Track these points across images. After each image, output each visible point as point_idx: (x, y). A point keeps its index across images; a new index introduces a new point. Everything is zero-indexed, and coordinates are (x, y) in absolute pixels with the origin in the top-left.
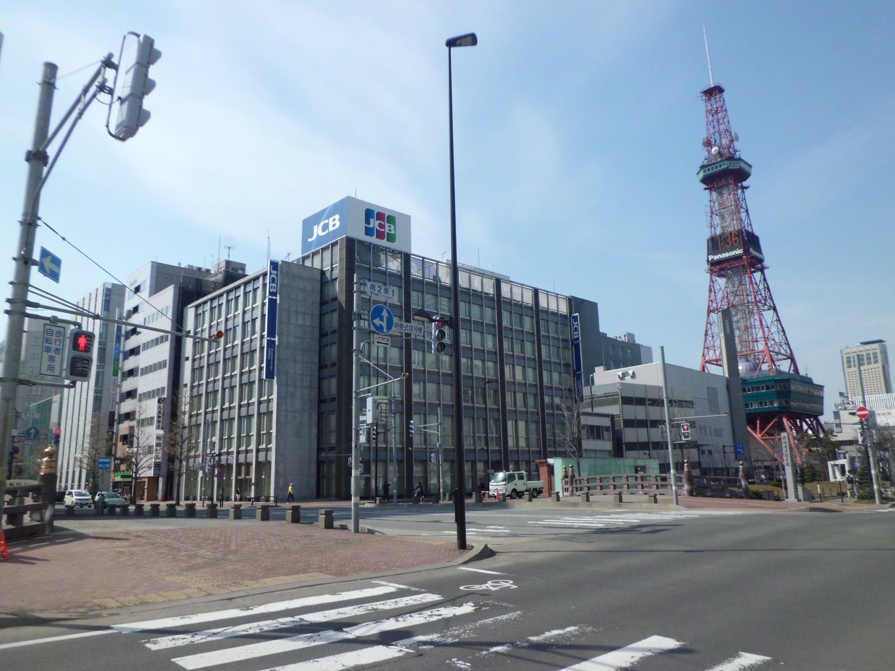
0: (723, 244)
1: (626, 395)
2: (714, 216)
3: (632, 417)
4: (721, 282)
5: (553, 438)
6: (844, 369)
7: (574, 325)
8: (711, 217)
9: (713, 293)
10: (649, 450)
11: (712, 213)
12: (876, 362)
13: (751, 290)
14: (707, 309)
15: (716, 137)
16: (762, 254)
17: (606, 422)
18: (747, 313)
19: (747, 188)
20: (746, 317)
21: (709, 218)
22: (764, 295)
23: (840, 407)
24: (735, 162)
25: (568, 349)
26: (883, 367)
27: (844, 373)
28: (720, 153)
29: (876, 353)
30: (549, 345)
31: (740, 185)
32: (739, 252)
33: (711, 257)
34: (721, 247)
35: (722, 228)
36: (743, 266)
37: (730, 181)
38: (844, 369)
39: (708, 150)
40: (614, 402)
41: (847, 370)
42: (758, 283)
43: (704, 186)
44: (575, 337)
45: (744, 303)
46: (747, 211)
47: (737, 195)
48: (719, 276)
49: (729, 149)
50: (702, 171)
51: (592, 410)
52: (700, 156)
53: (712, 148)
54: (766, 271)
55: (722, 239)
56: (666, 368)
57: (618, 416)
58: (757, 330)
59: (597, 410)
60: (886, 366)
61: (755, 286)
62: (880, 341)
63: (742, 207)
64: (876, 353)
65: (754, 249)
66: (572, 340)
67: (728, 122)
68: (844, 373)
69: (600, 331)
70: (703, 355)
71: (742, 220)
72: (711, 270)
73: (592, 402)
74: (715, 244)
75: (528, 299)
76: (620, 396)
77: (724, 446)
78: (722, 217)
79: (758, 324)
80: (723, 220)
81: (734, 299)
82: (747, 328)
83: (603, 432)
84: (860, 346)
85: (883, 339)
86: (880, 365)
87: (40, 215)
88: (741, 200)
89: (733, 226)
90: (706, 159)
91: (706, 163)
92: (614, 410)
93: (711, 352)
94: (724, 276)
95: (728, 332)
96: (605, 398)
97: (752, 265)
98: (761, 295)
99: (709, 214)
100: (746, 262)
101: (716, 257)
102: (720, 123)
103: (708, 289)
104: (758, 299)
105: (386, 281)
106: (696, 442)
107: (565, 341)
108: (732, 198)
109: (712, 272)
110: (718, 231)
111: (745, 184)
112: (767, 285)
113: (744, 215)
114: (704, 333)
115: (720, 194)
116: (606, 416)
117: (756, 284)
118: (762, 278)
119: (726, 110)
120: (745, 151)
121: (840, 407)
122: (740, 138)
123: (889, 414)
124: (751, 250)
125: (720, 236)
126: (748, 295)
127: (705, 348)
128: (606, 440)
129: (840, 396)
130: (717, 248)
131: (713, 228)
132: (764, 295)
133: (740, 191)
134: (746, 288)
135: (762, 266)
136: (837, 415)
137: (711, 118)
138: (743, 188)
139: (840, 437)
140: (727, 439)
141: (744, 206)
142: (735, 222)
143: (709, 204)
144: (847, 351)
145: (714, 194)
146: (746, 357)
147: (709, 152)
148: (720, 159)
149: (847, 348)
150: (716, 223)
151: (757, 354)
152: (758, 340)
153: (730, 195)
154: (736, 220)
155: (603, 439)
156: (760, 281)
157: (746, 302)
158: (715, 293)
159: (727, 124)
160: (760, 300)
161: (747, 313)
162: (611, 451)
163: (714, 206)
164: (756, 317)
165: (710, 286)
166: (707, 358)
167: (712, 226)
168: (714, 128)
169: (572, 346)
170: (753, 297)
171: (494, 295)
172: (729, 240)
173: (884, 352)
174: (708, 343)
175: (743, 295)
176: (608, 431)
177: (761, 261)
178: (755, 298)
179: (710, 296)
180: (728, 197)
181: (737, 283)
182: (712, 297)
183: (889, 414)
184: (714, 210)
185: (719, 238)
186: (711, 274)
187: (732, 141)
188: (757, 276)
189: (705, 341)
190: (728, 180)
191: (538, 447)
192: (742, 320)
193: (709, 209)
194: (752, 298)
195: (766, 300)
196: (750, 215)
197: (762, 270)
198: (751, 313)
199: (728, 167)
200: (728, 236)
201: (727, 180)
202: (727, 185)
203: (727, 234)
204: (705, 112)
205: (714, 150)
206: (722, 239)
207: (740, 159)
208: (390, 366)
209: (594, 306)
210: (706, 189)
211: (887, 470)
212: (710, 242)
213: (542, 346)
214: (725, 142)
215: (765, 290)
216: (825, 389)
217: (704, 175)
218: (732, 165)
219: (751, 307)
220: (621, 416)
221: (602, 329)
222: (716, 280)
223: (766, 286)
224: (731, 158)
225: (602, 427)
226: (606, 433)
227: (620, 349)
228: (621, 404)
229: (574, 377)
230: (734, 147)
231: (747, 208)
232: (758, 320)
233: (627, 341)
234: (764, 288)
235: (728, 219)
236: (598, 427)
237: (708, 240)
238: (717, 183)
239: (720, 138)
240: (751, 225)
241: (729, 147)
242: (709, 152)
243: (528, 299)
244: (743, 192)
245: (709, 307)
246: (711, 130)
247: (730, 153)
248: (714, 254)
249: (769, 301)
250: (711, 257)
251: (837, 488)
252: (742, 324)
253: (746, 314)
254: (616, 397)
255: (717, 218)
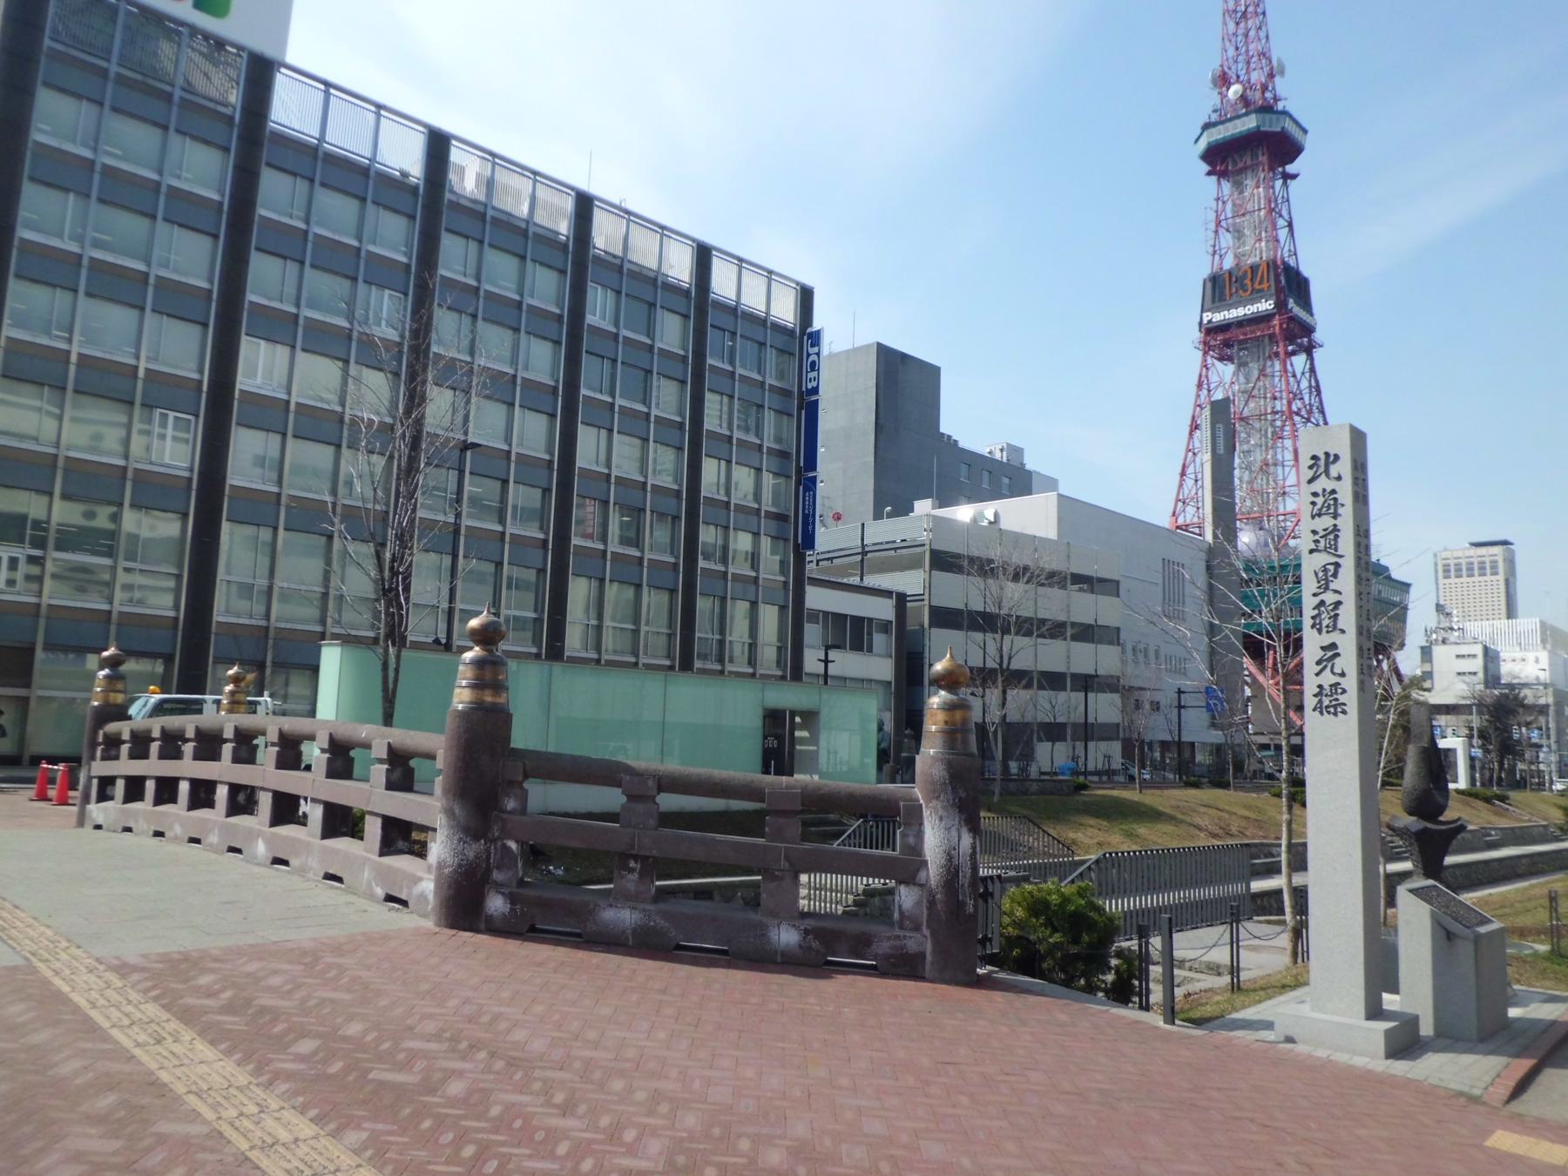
0: (1234, 290)
1: (941, 546)
2: (1221, 231)
3: (956, 603)
4: (1226, 370)
5: (717, 637)
6: (1437, 579)
7: (809, 355)
8: (1216, 232)
9: (1205, 392)
10: (375, 510)
11: (1218, 223)
12: (1496, 573)
13: (1284, 387)
14: (1189, 422)
15: (1240, 68)
16: (1312, 315)
17: (884, 610)
18: (1269, 435)
19: (1294, 177)
20: (1267, 443)
21: (1212, 235)
22: (1307, 402)
23: (1434, 636)
24: (1274, 117)
25: (790, 415)
26: (1507, 581)
27: (1437, 584)
28: (1243, 98)
29: (1496, 562)
30: (731, 397)
31: (1280, 169)
32: (1266, 306)
33: (1207, 316)
34: (1231, 295)
35: (1236, 256)
36: (1272, 337)
37: (1260, 159)
38: (1437, 579)
39: (1220, 93)
40: (913, 564)
41: (1442, 581)
42: (1299, 375)
43: (1205, 168)
44: (809, 387)
45: (1266, 414)
46: (1290, 225)
47: (1273, 187)
48: (1221, 359)
49: (1263, 93)
50: (1205, 134)
51: (862, 579)
52: (1206, 102)
53: (1228, 89)
54: (1317, 354)
55: (1234, 279)
56: (1068, 506)
57: (918, 598)
58: (1287, 469)
59: (872, 580)
60: (1511, 579)
61: (1292, 379)
62: (1505, 543)
63: (1281, 216)
64: (1496, 562)
65: (1295, 302)
66: (800, 392)
67: (1267, 37)
68: (1437, 584)
69: (942, 430)
70: (1174, 514)
71: (1278, 241)
72: (1205, 343)
73: (862, 561)
74: (1219, 288)
75: (680, 268)
76: (927, 547)
77: (1180, 692)
78: (1238, 234)
79: (1289, 456)
80: (1239, 239)
81: (1246, 404)
82: (1267, 465)
83: (870, 634)
84: (1468, 549)
85: (1510, 540)
86: (1501, 577)
87: (340, 372)
88: (1280, 201)
89: (1257, 252)
90: (1215, 111)
91: (1214, 117)
92: (911, 582)
93: (1190, 510)
94: (1230, 359)
95: (1221, 450)
96: (893, 552)
97: (1290, 337)
98: (1302, 399)
99: (1212, 226)
100: (1277, 328)
101: (1218, 317)
102: (1253, 66)
103: (1195, 381)
104: (1294, 408)
105: (761, 463)
106: (1118, 678)
107: (786, 393)
108: (1262, 195)
109: (1207, 347)
110: (1229, 263)
111: (1290, 168)
112: (1317, 381)
113: (1283, 234)
114: (1179, 470)
115: (1239, 186)
116: (887, 593)
117: (1294, 376)
118: (1308, 366)
119: (1264, 13)
120: (1294, 96)
121: (1434, 636)
122: (1288, 71)
123: (1524, 660)
124: (1291, 303)
125: (1230, 273)
126: (1275, 398)
127: (1178, 500)
128: (879, 655)
129: (1437, 611)
130: (1222, 299)
131: (1217, 257)
132: (1307, 402)
133: (1279, 183)
134: (1274, 387)
135: (1310, 341)
136: (1426, 653)
137: (1231, 26)
138: (1287, 177)
139: (1434, 699)
140: (1199, 673)
141: (1285, 213)
142: (1263, 244)
143: (1214, 204)
144: (1444, 555)
145: (1227, 187)
146: (1258, 523)
147: (1223, 96)
148: (1244, 111)
149: (1445, 550)
150: (1224, 244)
151: (1281, 518)
152: (1287, 490)
153: (1258, 187)
154: (1268, 241)
155: (870, 650)
156: (1303, 373)
157: (1269, 411)
158: (1209, 391)
159: (1264, 41)
160: (1299, 409)
161: (1269, 435)
162: (890, 683)
163: (1224, 210)
164: (1288, 443)
165: (1200, 375)
166: (1181, 521)
167: (1215, 252)
168: (1237, 49)
169: (800, 408)
170: (1285, 402)
171: (568, 238)
172: (1247, 281)
173: (1510, 562)
174: (1186, 492)
175: (1265, 398)
176: (886, 632)
177: (1308, 330)
178: (1290, 403)
179: (1198, 396)
180: (1255, 191)
181: (1256, 373)
182: (1202, 398)
183: (1524, 660)
184: (1223, 217)
185: (1227, 276)
186: (1205, 353)
187: (1271, 76)
188: (1299, 361)
189: (1181, 486)
190: (1257, 157)
191: (668, 657)
192: (1258, 449)
193: (1212, 216)
194: (1282, 405)
195: (1310, 412)
196: (1296, 235)
197: (1309, 350)
198: (1278, 436)
199: (1258, 127)
200: (1246, 272)
201: (1254, 156)
202: (1253, 168)
203: (1244, 268)
204: (1221, 13)
205: (1234, 90)
206: (1234, 279)
207: (1285, 113)
208: (732, 574)
209: (930, 374)
210: (1209, 174)
211: (832, 816)
212: (1209, 285)
213: (708, 396)
214: (1257, 77)
215: (1311, 393)
216: (1412, 590)
217: (1209, 143)
218: (1267, 124)
219: (1278, 423)
220: (926, 597)
221: (949, 424)
222: (1213, 364)
223: (1313, 384)
224: (1267, 109)
225: (870, 620)
226: (879, 640)
227: (986, 474)
228: (927, 568)
229: (798, 483)
230: (1274, 88)
231: (1291, 218)
232: (1291, 449)
233: (1005, 460)
234: (1310, 387)
235: (1250, 241)
236: (858, 621)
237: (1205, 281)
238: (1235, 163)
239: (1248, 69)
240: (1295, 254)
241: (1264, 88)
242: (1223, 96)
243: (680, 268)
244: (1285, 183)
245: (1193, 417)
246: (1231, 52)
247: (1265, 99)
248: (1215, 309)
249: (1317, 415)
250: (1207, 316)
251: (338, 622)
252: (1258, 457)
253: (1266, 437)
254: (918, 550)
255: (1228, 236)
